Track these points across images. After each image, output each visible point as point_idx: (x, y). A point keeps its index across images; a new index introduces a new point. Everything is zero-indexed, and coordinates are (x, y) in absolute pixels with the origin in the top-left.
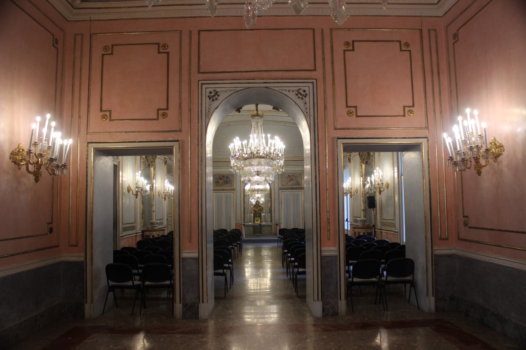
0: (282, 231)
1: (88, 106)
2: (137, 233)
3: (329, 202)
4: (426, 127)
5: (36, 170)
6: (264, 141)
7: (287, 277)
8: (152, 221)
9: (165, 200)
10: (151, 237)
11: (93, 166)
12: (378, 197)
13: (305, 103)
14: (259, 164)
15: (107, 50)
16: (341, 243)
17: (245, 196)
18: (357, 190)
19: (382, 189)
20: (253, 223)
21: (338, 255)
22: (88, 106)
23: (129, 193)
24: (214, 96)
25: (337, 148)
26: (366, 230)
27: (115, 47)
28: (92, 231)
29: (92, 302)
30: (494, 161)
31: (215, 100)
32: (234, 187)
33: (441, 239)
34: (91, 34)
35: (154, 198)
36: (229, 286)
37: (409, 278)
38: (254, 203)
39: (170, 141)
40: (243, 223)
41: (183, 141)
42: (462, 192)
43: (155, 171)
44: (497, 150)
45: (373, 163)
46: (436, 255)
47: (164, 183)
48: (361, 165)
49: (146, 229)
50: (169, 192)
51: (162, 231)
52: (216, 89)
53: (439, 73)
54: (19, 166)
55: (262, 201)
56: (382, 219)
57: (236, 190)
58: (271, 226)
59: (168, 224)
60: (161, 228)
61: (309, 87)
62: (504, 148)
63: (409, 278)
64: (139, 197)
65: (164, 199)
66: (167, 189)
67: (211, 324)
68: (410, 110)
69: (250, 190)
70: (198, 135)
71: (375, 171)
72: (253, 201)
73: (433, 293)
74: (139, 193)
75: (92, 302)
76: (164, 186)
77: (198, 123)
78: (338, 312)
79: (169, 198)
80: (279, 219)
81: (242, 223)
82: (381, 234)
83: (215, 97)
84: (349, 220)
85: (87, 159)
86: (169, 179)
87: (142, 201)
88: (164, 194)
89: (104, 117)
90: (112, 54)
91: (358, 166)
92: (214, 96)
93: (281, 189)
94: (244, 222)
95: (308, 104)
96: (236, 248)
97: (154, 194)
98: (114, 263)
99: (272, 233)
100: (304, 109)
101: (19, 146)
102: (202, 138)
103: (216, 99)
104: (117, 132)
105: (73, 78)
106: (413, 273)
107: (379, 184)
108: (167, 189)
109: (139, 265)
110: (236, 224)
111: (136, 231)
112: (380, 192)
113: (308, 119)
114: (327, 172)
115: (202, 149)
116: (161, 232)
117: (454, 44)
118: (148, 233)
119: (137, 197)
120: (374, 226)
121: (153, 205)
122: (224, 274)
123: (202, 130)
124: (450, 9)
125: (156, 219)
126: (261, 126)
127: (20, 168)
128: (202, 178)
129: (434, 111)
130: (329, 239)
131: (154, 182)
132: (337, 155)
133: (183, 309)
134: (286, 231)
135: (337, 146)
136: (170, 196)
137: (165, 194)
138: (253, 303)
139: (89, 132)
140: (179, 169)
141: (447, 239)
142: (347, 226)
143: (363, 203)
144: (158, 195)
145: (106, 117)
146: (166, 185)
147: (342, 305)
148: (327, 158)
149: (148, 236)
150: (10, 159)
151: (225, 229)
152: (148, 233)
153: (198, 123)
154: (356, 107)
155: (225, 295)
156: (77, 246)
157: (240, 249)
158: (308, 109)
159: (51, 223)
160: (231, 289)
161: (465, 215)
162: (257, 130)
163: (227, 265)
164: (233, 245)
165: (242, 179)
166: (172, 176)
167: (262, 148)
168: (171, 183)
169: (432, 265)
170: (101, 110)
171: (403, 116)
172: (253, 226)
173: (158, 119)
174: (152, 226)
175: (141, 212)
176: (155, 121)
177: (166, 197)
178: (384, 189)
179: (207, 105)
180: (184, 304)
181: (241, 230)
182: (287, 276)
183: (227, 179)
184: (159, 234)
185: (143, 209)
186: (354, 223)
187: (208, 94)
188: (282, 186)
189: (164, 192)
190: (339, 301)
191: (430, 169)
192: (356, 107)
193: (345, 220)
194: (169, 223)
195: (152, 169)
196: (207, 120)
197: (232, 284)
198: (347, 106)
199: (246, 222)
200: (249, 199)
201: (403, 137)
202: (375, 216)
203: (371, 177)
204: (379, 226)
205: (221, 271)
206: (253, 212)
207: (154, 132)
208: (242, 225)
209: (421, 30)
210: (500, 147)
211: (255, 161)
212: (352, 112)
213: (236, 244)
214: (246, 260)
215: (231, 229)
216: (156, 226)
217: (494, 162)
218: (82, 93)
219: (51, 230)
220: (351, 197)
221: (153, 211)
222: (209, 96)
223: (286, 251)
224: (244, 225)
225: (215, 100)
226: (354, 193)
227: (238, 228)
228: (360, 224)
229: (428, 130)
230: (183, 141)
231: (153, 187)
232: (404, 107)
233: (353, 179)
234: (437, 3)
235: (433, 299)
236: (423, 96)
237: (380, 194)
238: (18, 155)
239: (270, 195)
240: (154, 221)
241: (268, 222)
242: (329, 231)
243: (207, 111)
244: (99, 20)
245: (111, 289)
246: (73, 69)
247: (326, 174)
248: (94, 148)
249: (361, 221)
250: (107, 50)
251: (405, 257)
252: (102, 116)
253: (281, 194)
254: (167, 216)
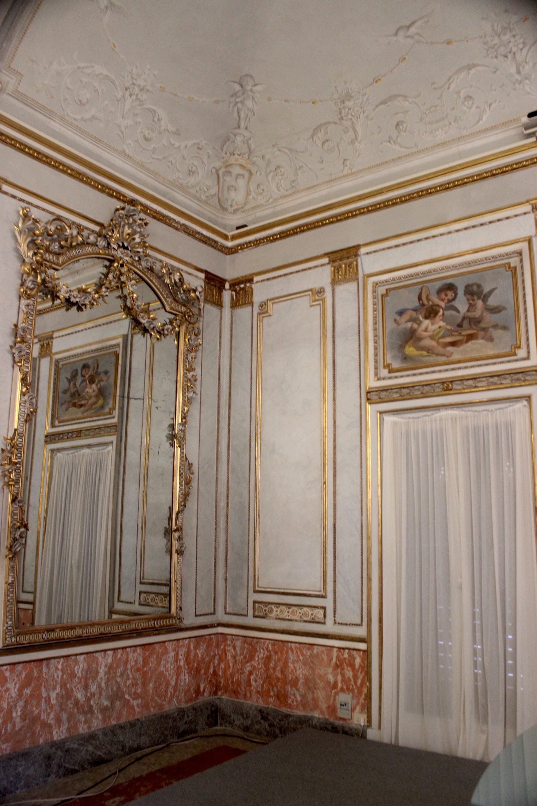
32: (528, 358)
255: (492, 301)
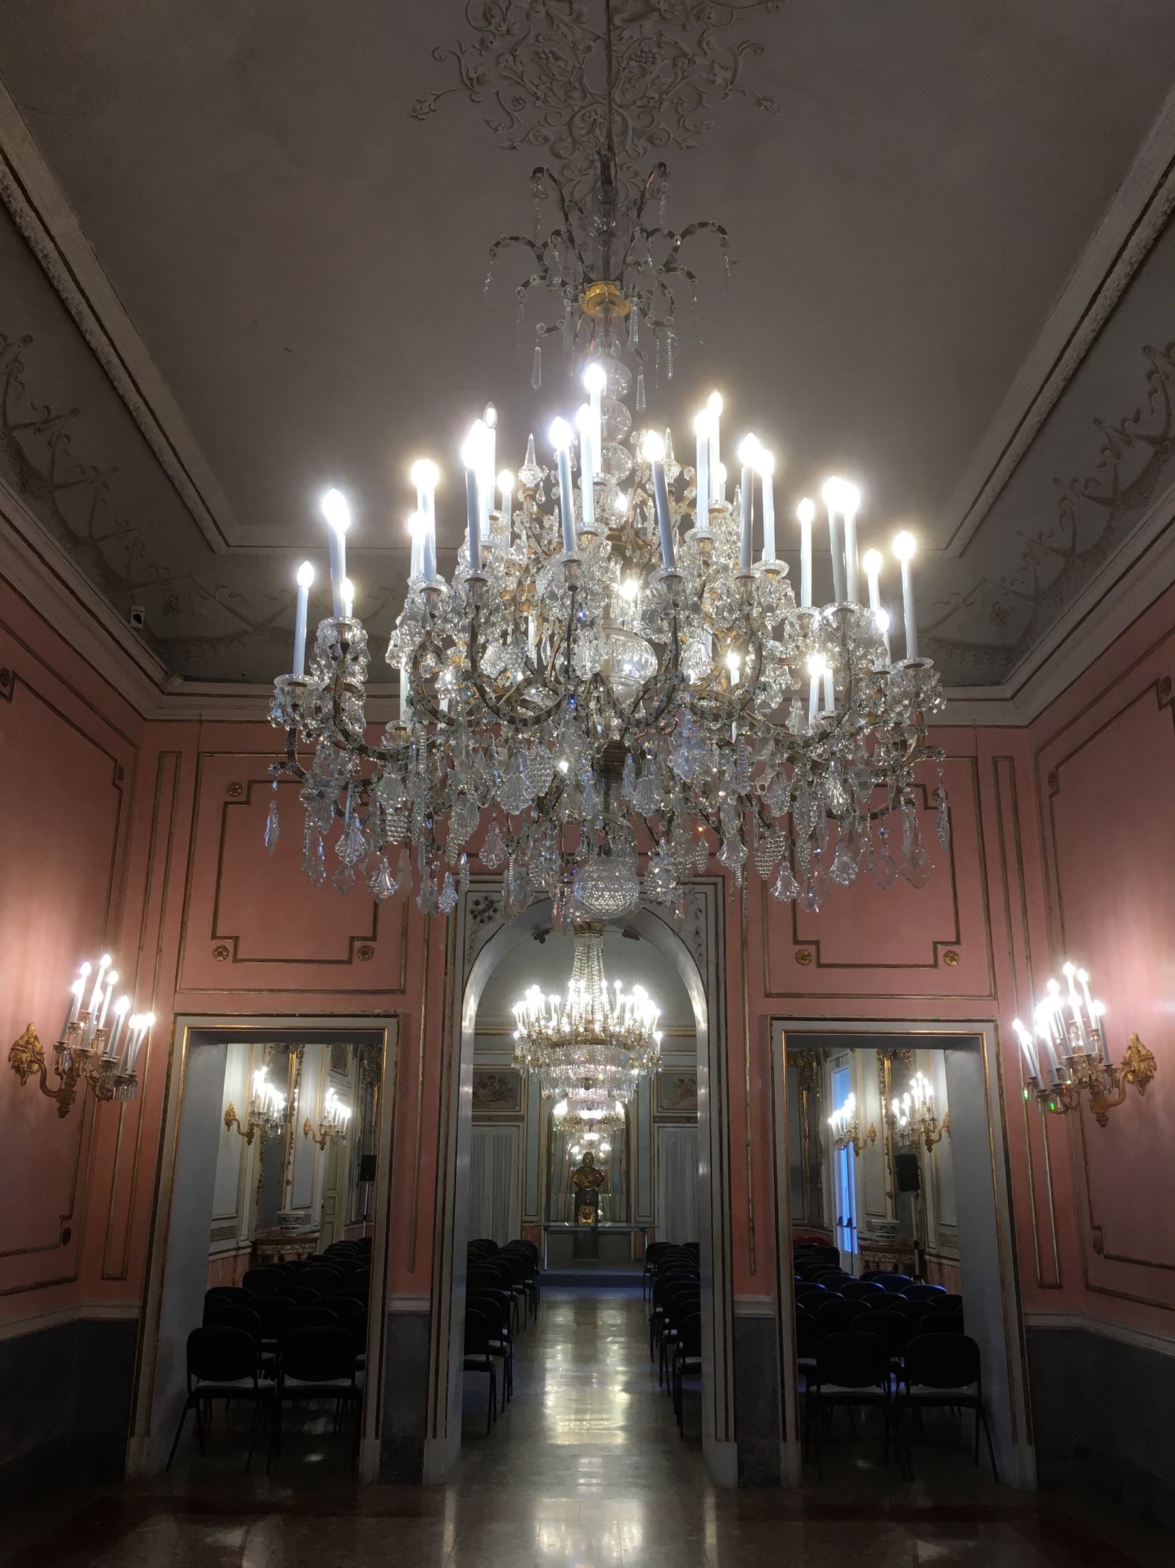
0: (657, 1252)
1: (183, 924)
2: (239, 1248)
3: (752, 1176)
4: (991, 996)
5: (63, 1087)
6: (605, 998)
7: (661, 1386)
8: (283, 1212)
9: (322, 1148)
10: (276, 1260)
11: (184, 1071)
12: (927, 1159)
13: (697, 933)
14: (592, 1060)
15: (236, 792)
16: (782, 1284)
17: (553, 1139)
18: (874, 1132)
19: (934, 1136)
20: (572, 1224)
21: (777, 1315)
22: (183, 924)
23: (229, 1130)
24: (484, 911)
25: (771, 1043)
26: (897, 1255)
27: (255, 787)
28: (166, 1240)
29: (148, 1432)
30: (1140, 1092)
31: (486, 919)
32: (520, 1111)
33: (1042, 1285)
34: (199, 753)
35: (294, 1141)
36: (499, 1406)
37: (967, 1390)
38: (579, 1157)
39: (378, 1016)
40: (543, 1221)
41: (408, 1016)
42: (1086, 1163)
43: (300, 1063)
44: (1142, 1066)
45: (910, 1057)
46: (1030, 1329)
47: (323, 1100)
48: (879, 1059)
49: (264, 1235)
50: (336, 1124)
51: (310, 1242)
52: (490, 894)
53: (1020, 863)
54: (23, 1077)
55: (604, 1152)
56: (941, 1225)
57: (525, 1122)
58: (628, 1234)
59: (323, 1222)
60: (306, 1233)
61: (706, 893)
62: (1155, 1063)
63: (967, 1390)
64: (256, 1140)
65: (318, 1146)
66: (331, 1116)
67: (451, 1504)
68: (950, 952)
69: (568, 1118)
70: (444, 1003)
71: (913, 1082)
72: (575, 1150)
73: (1029, 1437)
74: (256, 1131)
75: (148, 1432)
76: (322, 1109)
77: (446, 974)
78: (779, 1476)
79: (334, 1143)
80: (652, 1214)
81: (540, 1221)
82: (941, 1271)
83: (486, 914)
84: (854, 1225)
85: (171, 1054)
86: (340, 1087)
87: (261, 1153)
88: (320, 1131)
89: (220, 952)
90: (247, 802)
91: (875, 1064)
92: (484, 911)
93: (656, 1119)
94: (548, 1219)
95: (703, 935)
96: (521, 1298)
97: (294, 1131)
98: (203, 1325)
99: (630, 1257)
100: (693, 947)
101: (28, 1029)
102: (452, 1011)
103: (490, 918)
104: (248, 990)
105: (150, 856)
106: (978, 1378)
107: (923, 1121)
108: (331, 1116)
109: (264, 1341)
110: (524, 1225)
111: (237, 1243)
112: (929, 1143)
113: (704, 971)
114: (749, 1099)
115: (451, 1036)
116: (307, 1245)
117: (1051, 796)
118: (268, 1247)
119: (249, 1142)
120: (917, 1244)
121: (289, 1163)
122: (486, 1367)
123: (453, 990)
124: (1041, 713)
125: (291, 1205)
126: (598, 956)
127: (25, 1082)
128: (448, 1107)
129: (1012, 954)
130: (753, 1273)
131: (296, 1096)
132: (772, 1059)
133: (382, 1455)
134: (668, 1250)
135: (772, 1038)
136: (337, 1136)
137: (323, 1132)
138: (565, 1485)
139: (180, 989)
140: (395, 1085)
141: (1060, 1287)
142: (847, 1242)
143: (890, 1173)
144: (302, 1132)
145: (225, 954)
146: (327, 1104)
147: (790, 1454)
148: (748, 1065)
149: (266, 1258)
150: (10, 1060)
151: (490, 1239)
152: (269, 1250)
153: (446, 974)
154: (817, 943)
155: (489, 1429)
156: (125, 1279)
157: (534, 1304)
158: (704, 947)
159: (69, 1217)
160: (505, 1413)
161: (1096, 1223)
162: (588, 967)
163: (497, 1343)
164: (512, 1290)
165: (545, 1093)
166: (346, 1076)
167: (599, 1016)
168: (343, 1095)
169: (1022, 1355)
170: (214, 936)
171: (931, 966)
172: (574, 1233)
173: (349, 962)
174: (282, 1228)
175: (256, 1184)
176: (342, 967)
177: (328, 1139)
178: (940, 1136)
179: (468, 933)
180: (384, 1442)
181: (537, 1245)
182: (659, 1385)
183: (501, 1087)
184: (301, 1251)
185: (261, 1176)
186: (867, 1235)
187: (470, 906)
188: (660, 1110)
189: (321, 1125)
190: (782, 1445)
191: (1003, 1100)
192: (817, 943)
193: (845, 1223)
194: (328, 1219)
195: (295, 1056)
196: (467, 968)
197: (509, 1401)
198: (796, 942)
199: (551, 1219)
200: (565, 1144)
201: (933, 1018)
202: (922, 1213)
203: (901, 1101)
204: (934, 1246)
205: (482, 1358)
206: (575, 1189)
207: (341, 992)
208: (540, 1231)
209: (976, 758)
210: (1148, 1059)
211: (579, 1054)
212: (809, 955)
213: (521, 1287)
214: (550, 1337)
215: (509, 1242)
216: (294, 1228)
217: (1139, 1095)
218: (170, 892)
219: (66, 1236)
220: (857, 1154)
221: (288, 1183)
222: (472, 912)
223: (659, 1310)
224: (546, 1228)
225: (486, 919)
226: (866, 1141)
227: (529, 1238)
228: (882, 1236)
229: (996, 1002)
230: (408, 1016)
231: (294, 1109)
232: (935, 943)
233: (862, 1100)
234: (1012, 698)
235: (1029, 1452)
236: (983, 917)
237: (930, 1150)
238: (24, 1052)
239: (624, 1135)
240: (287, 1210)
241: (619, 1222)
242: (753, 1250)
243: (467, 947)
244: (219, 721)
245: (194, 1398)
246: (152, 836)
247: (746, 1105)
248: (189, 1028)
249: (882, 1228)
250: (236, 792)
251: (963, 1333)
252: (214, 951)
253: (659, 1134)
254: (324, 1197)
255: (509, 1086)
